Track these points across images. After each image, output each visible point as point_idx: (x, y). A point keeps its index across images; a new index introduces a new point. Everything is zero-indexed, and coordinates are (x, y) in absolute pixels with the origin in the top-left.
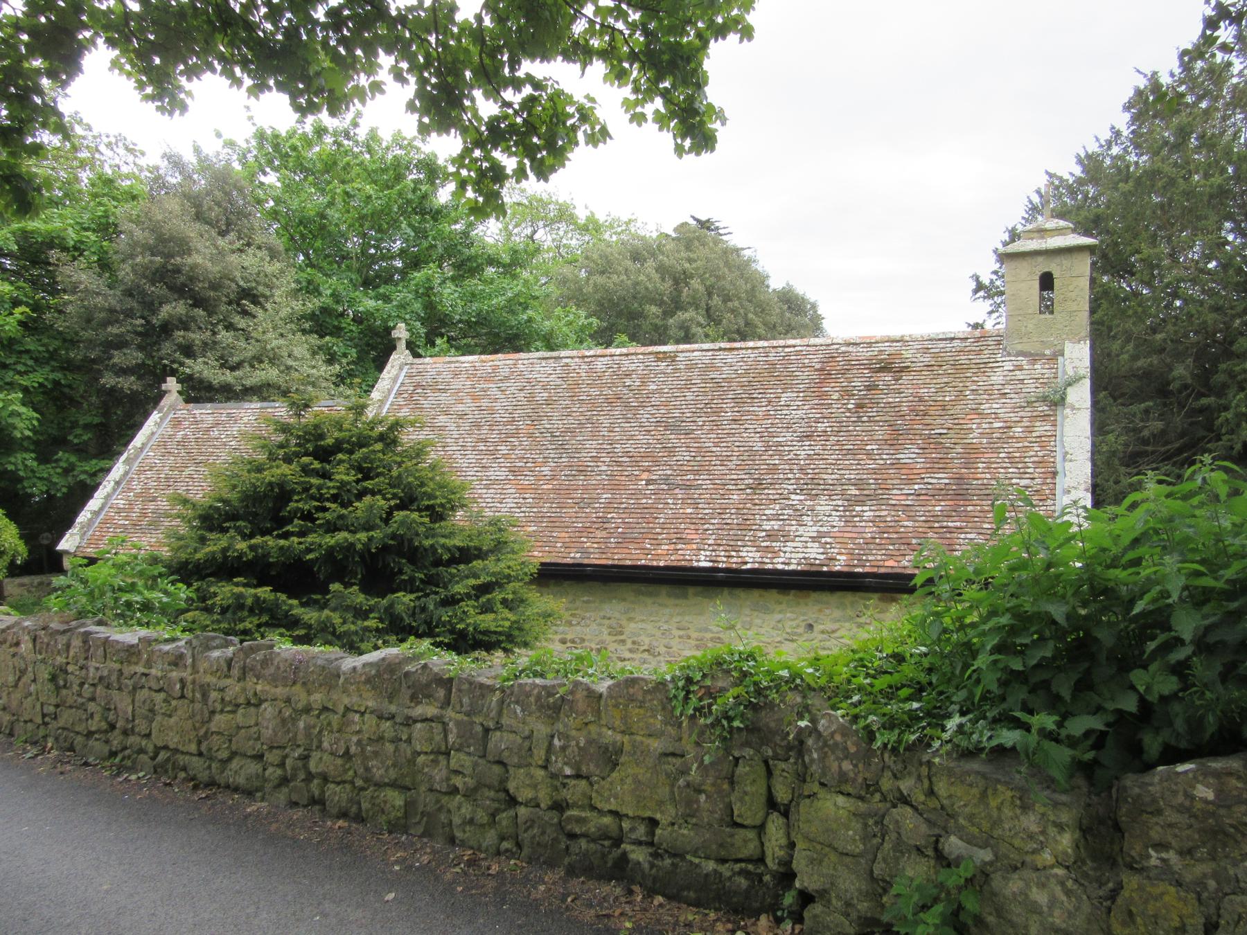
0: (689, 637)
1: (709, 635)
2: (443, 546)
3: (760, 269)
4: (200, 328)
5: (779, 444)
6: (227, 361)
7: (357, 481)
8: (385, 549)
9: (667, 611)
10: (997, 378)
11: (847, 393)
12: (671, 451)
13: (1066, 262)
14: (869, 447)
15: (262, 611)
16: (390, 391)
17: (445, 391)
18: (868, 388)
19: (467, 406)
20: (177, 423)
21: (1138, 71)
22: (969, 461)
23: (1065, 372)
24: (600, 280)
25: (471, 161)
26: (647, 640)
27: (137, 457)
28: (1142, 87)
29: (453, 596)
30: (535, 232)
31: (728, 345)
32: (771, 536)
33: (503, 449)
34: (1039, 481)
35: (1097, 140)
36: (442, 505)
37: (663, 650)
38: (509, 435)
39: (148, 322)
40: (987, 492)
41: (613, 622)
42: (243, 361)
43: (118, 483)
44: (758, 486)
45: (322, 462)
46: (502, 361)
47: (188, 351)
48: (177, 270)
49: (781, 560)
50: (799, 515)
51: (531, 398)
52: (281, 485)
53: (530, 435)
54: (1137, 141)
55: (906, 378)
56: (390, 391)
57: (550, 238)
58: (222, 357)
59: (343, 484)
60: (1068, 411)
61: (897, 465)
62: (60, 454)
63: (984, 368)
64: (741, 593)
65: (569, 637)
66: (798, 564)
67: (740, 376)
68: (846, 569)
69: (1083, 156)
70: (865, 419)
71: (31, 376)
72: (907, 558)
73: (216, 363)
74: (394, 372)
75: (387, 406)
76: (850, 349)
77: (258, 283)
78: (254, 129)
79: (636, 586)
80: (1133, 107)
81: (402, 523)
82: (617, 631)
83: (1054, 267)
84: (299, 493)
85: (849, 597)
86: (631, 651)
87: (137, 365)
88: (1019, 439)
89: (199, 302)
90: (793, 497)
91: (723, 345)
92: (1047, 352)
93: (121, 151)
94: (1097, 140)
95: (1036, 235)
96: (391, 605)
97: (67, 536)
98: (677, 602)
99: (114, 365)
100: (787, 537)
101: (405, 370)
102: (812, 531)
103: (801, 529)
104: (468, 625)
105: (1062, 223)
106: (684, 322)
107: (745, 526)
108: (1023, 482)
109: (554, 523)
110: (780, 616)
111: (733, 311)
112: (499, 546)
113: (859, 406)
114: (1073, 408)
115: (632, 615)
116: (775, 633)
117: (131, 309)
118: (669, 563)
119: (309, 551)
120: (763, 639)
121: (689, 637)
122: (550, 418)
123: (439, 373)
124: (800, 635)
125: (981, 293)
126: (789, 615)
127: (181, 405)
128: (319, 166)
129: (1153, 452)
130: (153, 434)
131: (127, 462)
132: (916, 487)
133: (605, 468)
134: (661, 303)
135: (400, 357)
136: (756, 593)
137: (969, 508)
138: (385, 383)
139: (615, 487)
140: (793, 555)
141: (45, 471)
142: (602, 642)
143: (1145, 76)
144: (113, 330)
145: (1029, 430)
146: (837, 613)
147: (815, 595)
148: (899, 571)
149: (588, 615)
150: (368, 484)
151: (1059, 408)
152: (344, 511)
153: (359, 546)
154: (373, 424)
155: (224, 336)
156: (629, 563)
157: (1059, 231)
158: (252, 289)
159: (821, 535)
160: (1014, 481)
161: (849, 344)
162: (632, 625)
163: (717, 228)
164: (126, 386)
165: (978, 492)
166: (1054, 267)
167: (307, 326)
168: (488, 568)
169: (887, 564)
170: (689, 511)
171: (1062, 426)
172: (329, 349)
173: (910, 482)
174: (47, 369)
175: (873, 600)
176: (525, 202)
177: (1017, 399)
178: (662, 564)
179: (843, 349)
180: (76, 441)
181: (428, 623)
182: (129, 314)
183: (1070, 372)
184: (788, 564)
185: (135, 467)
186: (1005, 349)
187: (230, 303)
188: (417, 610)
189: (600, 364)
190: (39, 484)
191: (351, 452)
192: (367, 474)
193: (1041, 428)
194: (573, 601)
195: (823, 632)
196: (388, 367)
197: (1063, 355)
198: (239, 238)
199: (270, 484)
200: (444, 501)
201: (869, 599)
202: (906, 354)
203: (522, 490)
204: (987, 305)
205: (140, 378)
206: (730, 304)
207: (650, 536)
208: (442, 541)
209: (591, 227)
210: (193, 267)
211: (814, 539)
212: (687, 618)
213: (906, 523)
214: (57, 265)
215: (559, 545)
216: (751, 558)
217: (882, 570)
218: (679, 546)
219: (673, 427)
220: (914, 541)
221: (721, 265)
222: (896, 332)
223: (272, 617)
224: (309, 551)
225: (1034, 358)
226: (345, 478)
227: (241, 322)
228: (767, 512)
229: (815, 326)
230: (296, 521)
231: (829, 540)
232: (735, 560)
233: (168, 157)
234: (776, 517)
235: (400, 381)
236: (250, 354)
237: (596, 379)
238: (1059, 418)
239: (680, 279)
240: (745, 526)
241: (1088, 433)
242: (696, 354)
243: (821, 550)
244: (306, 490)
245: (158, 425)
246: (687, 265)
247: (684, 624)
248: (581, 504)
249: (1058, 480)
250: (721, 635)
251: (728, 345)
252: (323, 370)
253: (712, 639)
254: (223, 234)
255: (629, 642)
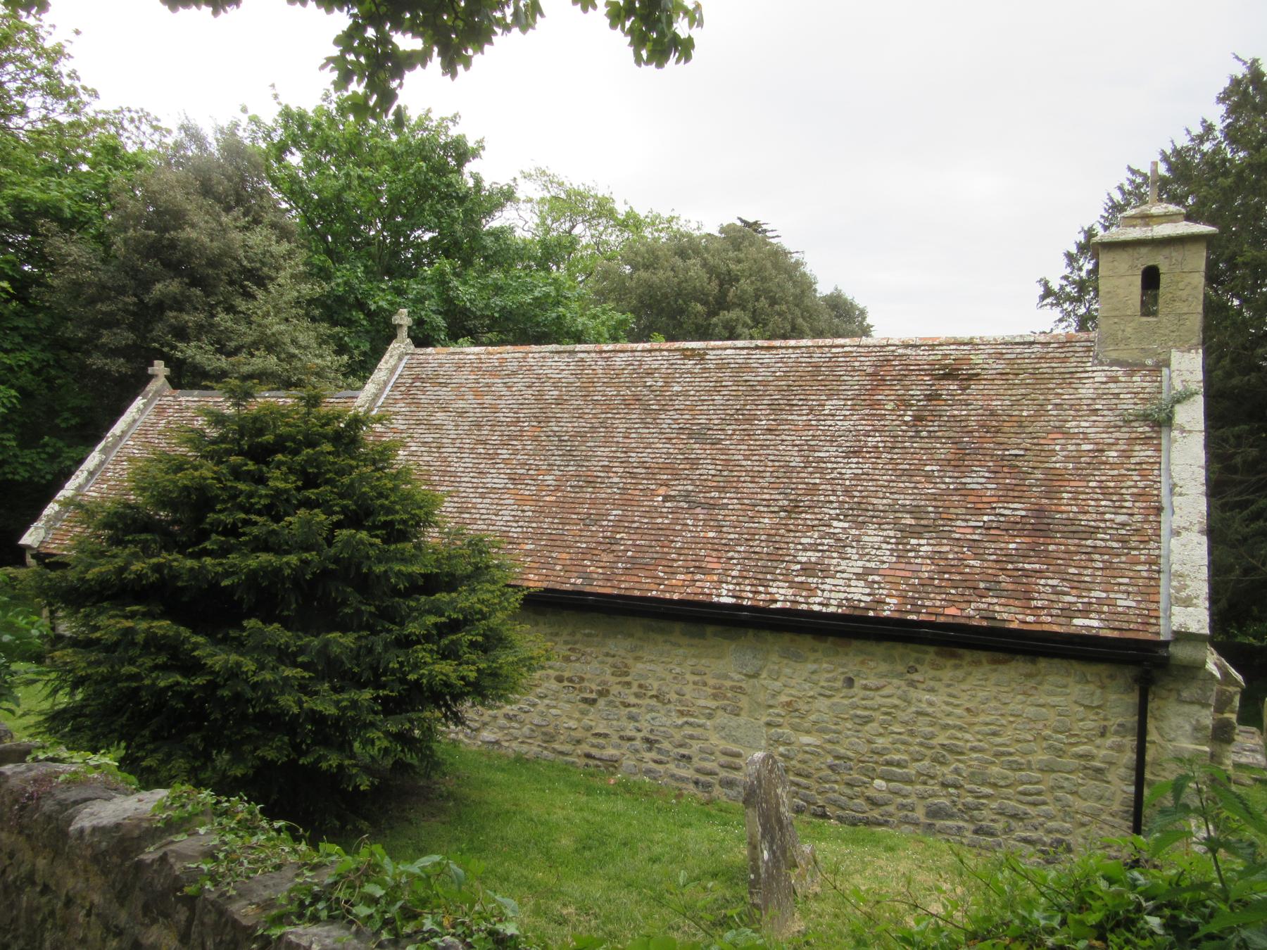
0: (705, 684)
1: (728, 683)
2: (399, 574)
3: (808, 272)
4: (197, 309)
5: (821, 460)
6: (223, 346)
7: (298, 489)
8: (325, 573)
9: (681, 651)
10: (1086, 391)
11: (904, 403)
12: (694, 463)
13: (1175, 254)
14: (928, 468)
15: (160, 649)
16: (386, 383)
17: (446, 385)
18: (929, 398)
19: (467, 402)
20: (161, 411)
21: (1237, 57)
22: (1052, 489)
23: (1171, 387)
24: (643, 274)
25: (361, 44)
26: (656, 685)
27: (115, 445)
28: (1240, 76)
29: (407, 636)
30: (573, 227)
31: (766, 343)
32: (807, 569)
33: (503, 452)
34: (1138, 518)
35: (1189, 132)
36: (404, 522)
37: (674, 697)
38: (511, 438)
39: (141, 301)
40: (1074, 528)
41: (617, 660)
42: (242, 347)
43: (91, 474)
44: (793, 509)
45: (257, 462)
46: (510, 353)
47: (181, 333)
48: (173, 245)
49: (818, 600)
50: (841, 546)
51: (539, 397)
52: (202, 489)
53: (535, 439)
54: (1232, 134)
55: (974, 387)
56: (386, 383)
57: (588, 233)
58: (218, 342)
59: (278, 492)
60: (1175, 433)
61: (962, 491)
62: (46, 438)
63: (1069, 379)
64: (769, 636)
65: (566, 674)
66: (839, 606)
67: (778, 379)
68: (896, 615)
69: (1169, 151)
70: (924, 434)
71: (18, 354)
72: (973, 605)
73: (209, 348)
74: (393, 362)
75: (382, 400)
76: (908, 351)
77: (263, 264)
78: (279, 109)
79: (646, 621)
80: (1228, 98)
81: (347, 543)
82: (621, 671)
83: (1160, 260)
84: (224, 501)
85: (899, 649)
86: (637, 695)
87: (127, 346)
88: (1113, 466)
89: (195, 281)
90: (835, 523)
91: (760, 343)
92: (1149, 362)
93: (145, 127)
94: (1189, 132)
95: (1139, 221)
96: (326, 644)
97: (32, 529)
98: (696, 641)
99: (103, 345)
100: (826, 572)
101: (405, 361)
102: (857, 566)
103: (843, 563)
104: (422, 676)
105: (1172, 208)
106: (727, 322)
107: (776, 557)
108: (1120, 519)
109: (555, 542)
110: (814, 667)
111: (779, 314)
112: (479, 572)
113: (918, 418)
114: (1183, 430)
115: (640, 653)
116: (807, 686)
117: (124, 286)
118: (684, 596)
119: (227, 574)
120: (793, 692)
121: (705, 684)
122: (558, 420)
123: (441, 365)
124: (837, 690)
125: (1049, 300)
126: (825, 665)
127: (168, 390)
128: (345, 147)
129: (1241, 482)
130: (135, 421)
131: (103, 451)
132: (986, 518)
133: (616, 480)
134: (705, 303)
135: (401, 346)
136: (787, 637)
137: (1051, 548)
138: (382, 374)
139: (626, 502)
140: (833, 595)
141: (29, 456)
142: (604, 683)
143: (1245, 63)
144: (102, 307)
145: (1126, 454)
146: (884, 667)
147: (856, 644)
148: (963, 621)
149: (588, 650)
150: (311, 493)
151: (1164, 430)
152: (275, 526)
153: (287, 572)
154: (328, 420)
155: (223, 319)
156: (637, 593)
157: (1168, 218)
158: (257, 270)
159: (867, 572)
160: (1107, 516)
161: (906, 346)
162: (640, 665)
163: (765, 231)
164: (114, 368)
165: (1061, 528)
166: (1160, 260)
167: (317, 312)
168: (464, 600)
169: (947, 611)
170: (711, 534)
171: (1169, 451)
172: (341, 339)
173: (978, 512)
174: (39, 347)
175: (930, 653)
176: (563, 196)
177: (1110, 417)
178: (676, 597)
179: (901, 351)
180: (63, 425)
181: (374, 669)
182: (121, 291)
183: (1179, 387)
184: (827, 605)
185: (112, 457)
186: (1096, 357)
187: (231, 283)
188: (363, 651)
189: (619, 360)
190: (21, 470)
191: (296, 452)
192: (310, 481)
193: (1142, 453)
194: (573, 634)
195: (866, 688)
196: (387, 356)
197: (1168, 366)
198: (245, 215)
199: (186, 487)
200: (405, 517)
201: (927, 653)
202: (976, 359)
203: (521, 501)
204: (1056, 313)
205: (128, 360)
206: (777, 307)
207: (664, 563)
208: (397, 567)
209: (631, 223)
210: (189, 241)
211: (859, 576)
212: (703, 661)
213: (972, 562)
214: (46, 236)
215: (558, 568)
216: (781, 595)
217: (942, 619)
218: (698, 577)
219: (700, 435)
220: (982, 585)
221: (769, 265)
222: (964, 335)
223: (174, 656)
224: (227, 574)
225: (1133, 368)
226: (281, 485)
227: (242, 305)
228: (804, 541)
229: (866, 332)
230: (214, 537)
231: (877, 578)
232: (763, 596)
233: (185, 128)
234: (814, 547)
235: (398, 372)
236: (249, 339)
237: (613, 377)
238: (1163, 442)
239: (728, 279)
240: (776, 557)
241: (1203, 462)
242: (728, 352)
243: (868, 591)
244: (233, 497)
245: (141, 411)
246: (732, 266)
247: (699, 668)
248: (588, 520)
249: (1163, 518)
250: (743, 685)
251: (766, 343)
252: (329, 359)
253: (732, 688)
254: (228, 209)
255: (635, 685)
